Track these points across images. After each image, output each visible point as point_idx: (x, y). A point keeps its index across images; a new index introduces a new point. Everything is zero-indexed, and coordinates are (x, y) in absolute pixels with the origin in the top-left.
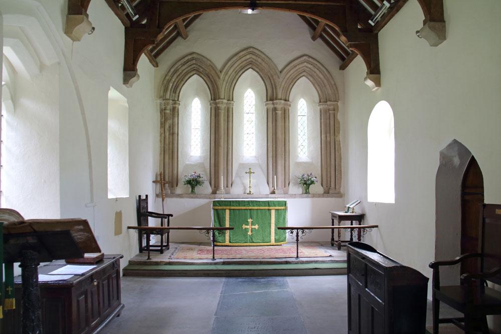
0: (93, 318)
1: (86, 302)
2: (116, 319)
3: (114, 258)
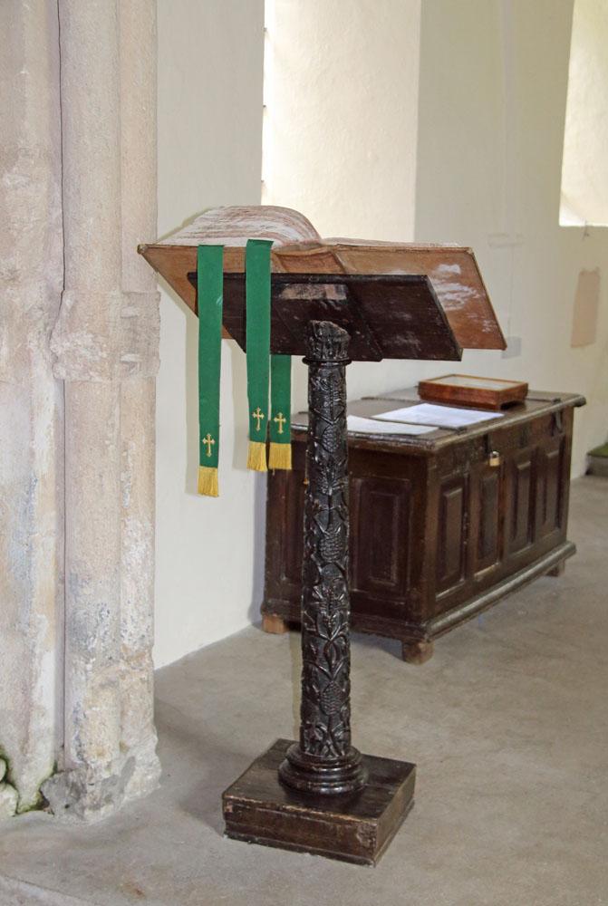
0: (482, 554)
1: (465, 508)
2: (544, 580)
3: (557, 401)
